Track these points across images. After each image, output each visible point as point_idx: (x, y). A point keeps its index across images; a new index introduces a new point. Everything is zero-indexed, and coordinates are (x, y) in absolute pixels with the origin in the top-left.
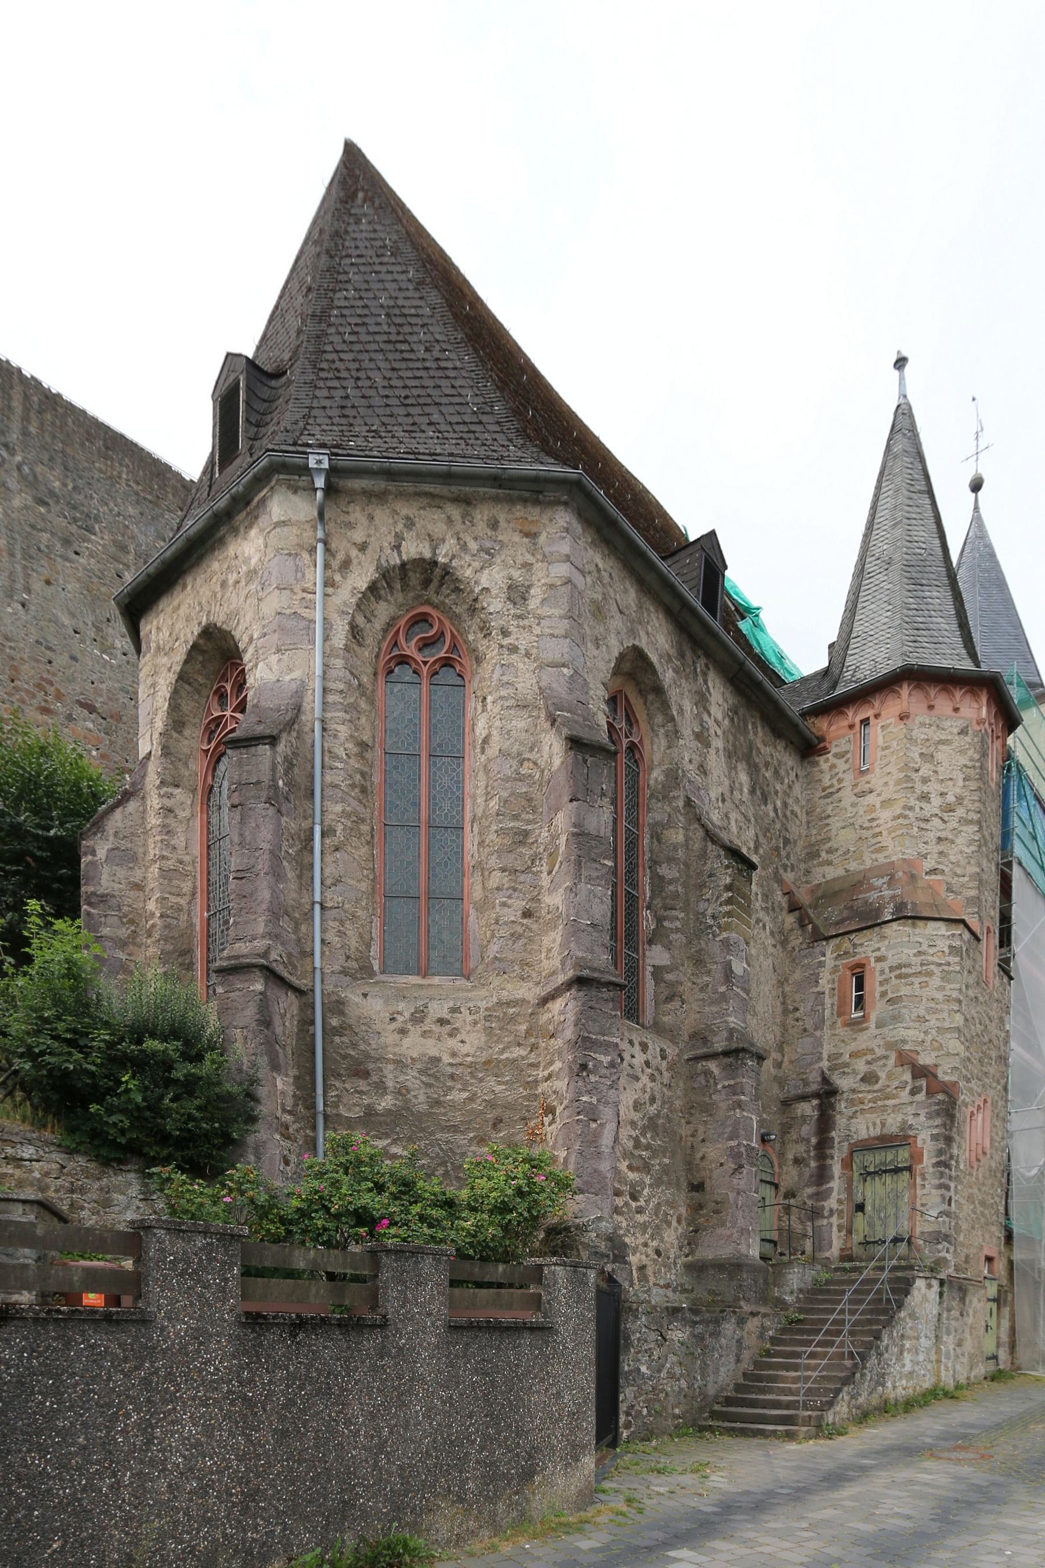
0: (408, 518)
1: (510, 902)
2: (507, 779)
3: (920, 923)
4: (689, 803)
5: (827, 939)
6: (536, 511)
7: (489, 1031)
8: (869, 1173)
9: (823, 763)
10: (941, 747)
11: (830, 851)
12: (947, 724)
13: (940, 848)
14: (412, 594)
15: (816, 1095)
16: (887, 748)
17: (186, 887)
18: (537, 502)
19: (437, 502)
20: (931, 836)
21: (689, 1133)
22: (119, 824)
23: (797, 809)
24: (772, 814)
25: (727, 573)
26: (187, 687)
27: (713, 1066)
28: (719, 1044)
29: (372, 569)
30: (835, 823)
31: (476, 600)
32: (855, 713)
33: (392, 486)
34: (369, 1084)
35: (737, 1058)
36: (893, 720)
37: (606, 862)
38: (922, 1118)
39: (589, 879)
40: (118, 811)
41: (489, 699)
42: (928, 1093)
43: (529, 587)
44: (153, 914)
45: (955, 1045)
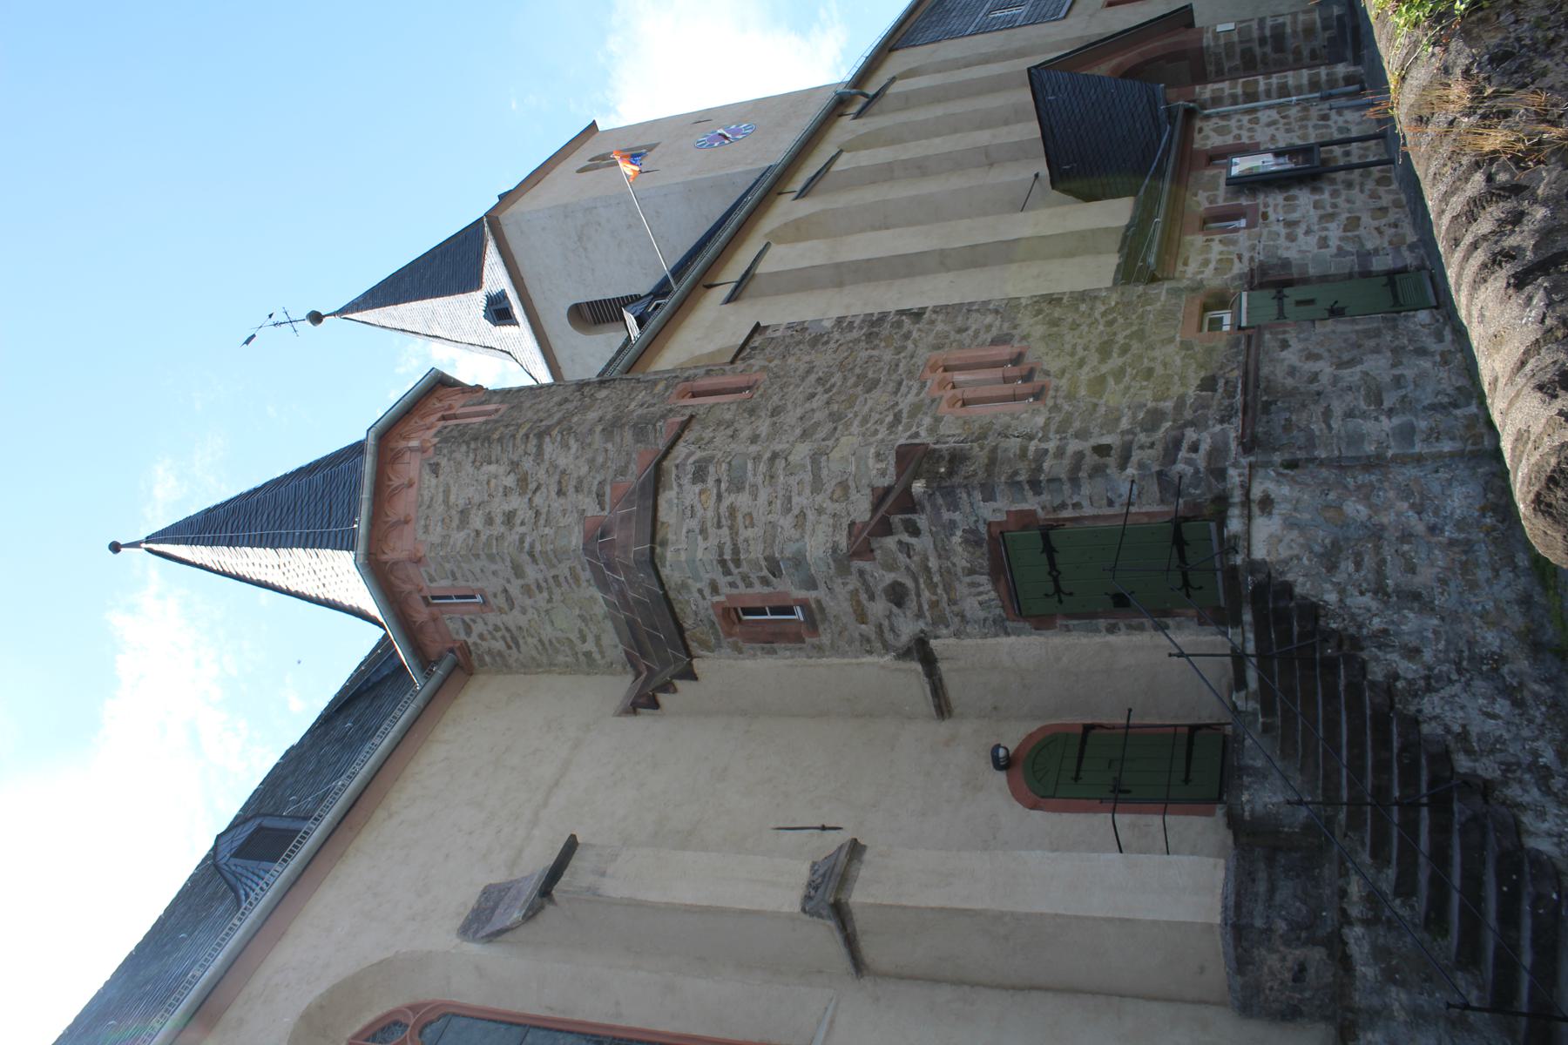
10: (452, 498)
12: (426, 495)
13: (571, 490)
20: (557, 503)
42: (914, 511)
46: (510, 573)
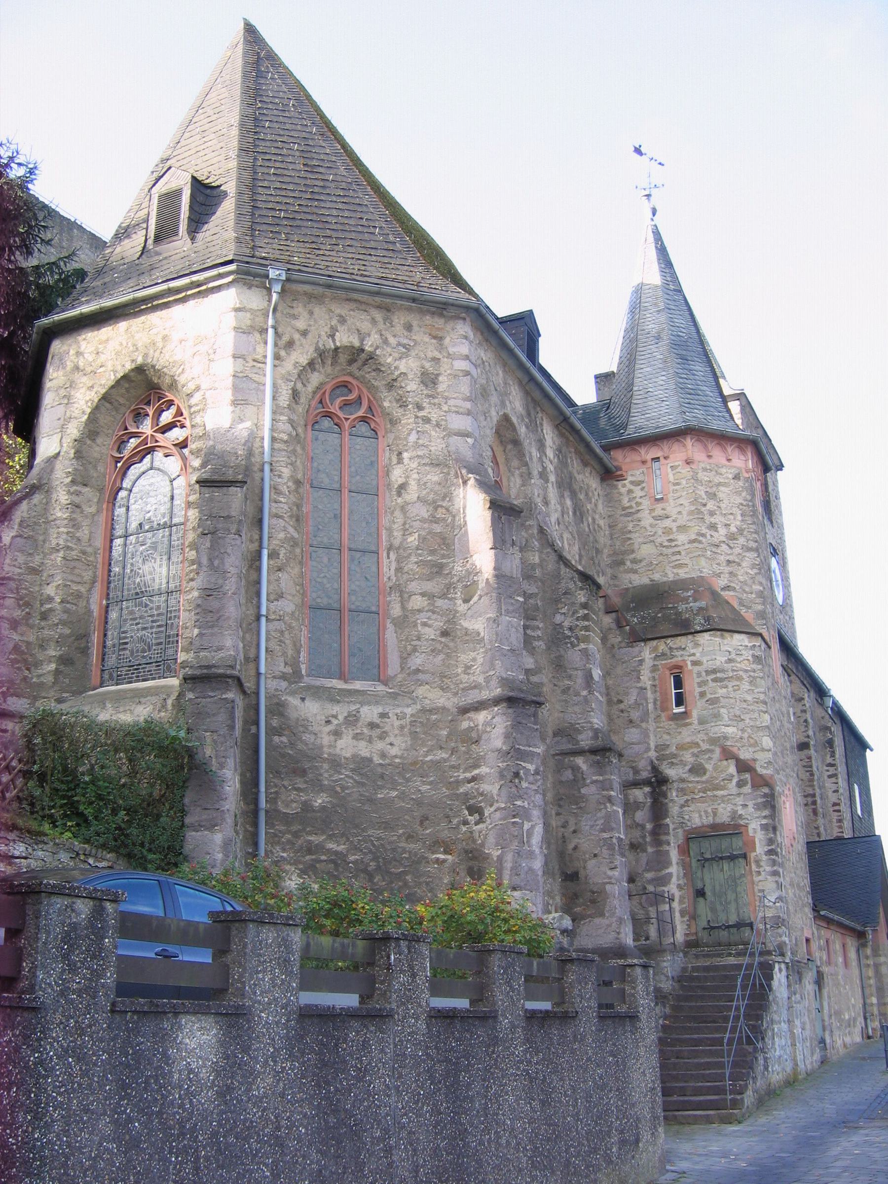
0: (341, 316)
1: (430, 622)
2: (423, 520)
3: (726, 634)
4: (541, 531)
5: (646, 640)
6: (442, 321)
7: (414, 735)
8: (707, 860)
9: (623, 487)
10: (722, 488)
11: (635, 561)
12: (723, 470)
13: (731, 569)
14: (338, 368)
15: (647, 782)
16: (678, 484)
17: (87, 575)
18: (441, 315)
19: (364, 307)
20: (722, 559)
21: (559, 824)
22: (25, 515)
23: (601, 523)
24: (587, 529)
25: (540, 339)
26: (108, 405)
27: (580, 761)
28: (585, 740)
29: (312, 349)
30: (637, 538)
31: (395, 380)
32: (647, 452)
33: (328, 292)
34: (306, 782)
35: (604, 756)
36: (680, 463)
37: (519, 598)
38: (751, 809)
39: (508, 612)
40: (25, 502)
41: (405, 455)
42: (753, 786)
43: (438, 375)
44: (50, 599)
45: (767, 742)
46: (680, 522)
